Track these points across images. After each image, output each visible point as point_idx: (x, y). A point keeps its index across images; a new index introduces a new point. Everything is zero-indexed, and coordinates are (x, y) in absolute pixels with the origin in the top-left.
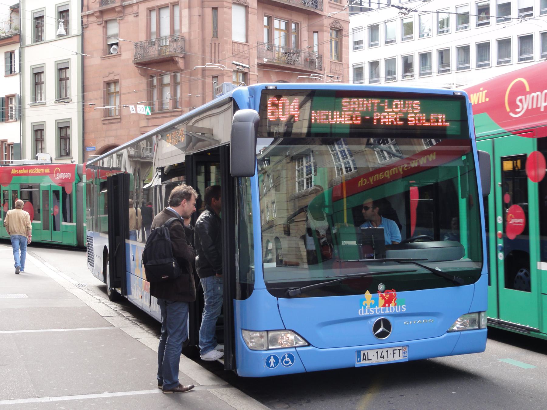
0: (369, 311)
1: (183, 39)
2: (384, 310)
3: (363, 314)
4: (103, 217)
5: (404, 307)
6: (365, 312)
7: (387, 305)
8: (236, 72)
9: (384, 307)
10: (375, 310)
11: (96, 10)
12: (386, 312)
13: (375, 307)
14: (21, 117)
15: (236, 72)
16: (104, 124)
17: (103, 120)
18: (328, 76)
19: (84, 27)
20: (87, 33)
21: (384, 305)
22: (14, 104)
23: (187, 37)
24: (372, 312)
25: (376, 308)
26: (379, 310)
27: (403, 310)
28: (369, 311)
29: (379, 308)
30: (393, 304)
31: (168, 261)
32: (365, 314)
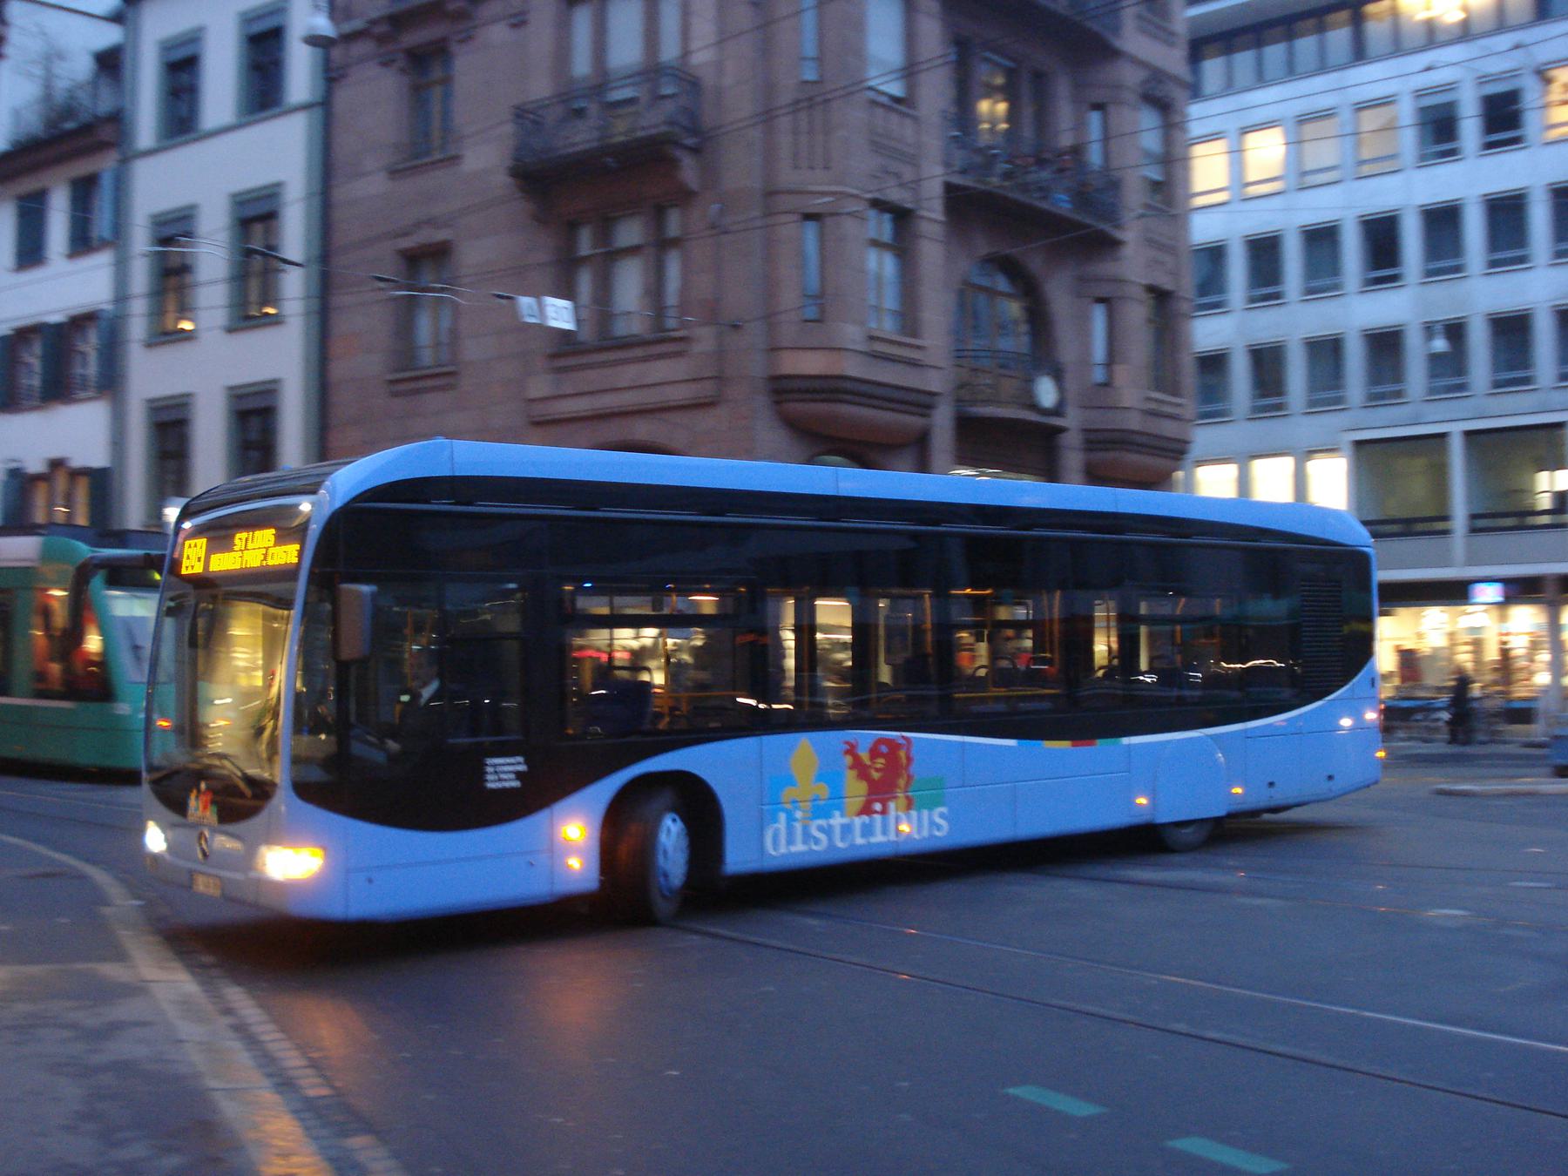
0: (807, 836)
1: (692, 84)
2: (867, 831)
3: (783, 850)
4: (833, 713)
5: (942, 816)
6: (790, 842)
7: (878, 807)
8: (879, 205)
9: (865, 818)
10: (828, 831)
11: (374, 14)
12: (873, 840)
13: (828, 816)
14: (111, 383)
15: (879, 205)
16: (396, 395)
17: (392, 382)
18: (1376, 782)
19: (331, 76)
20: (345, 96)
21: (866, 810)
22: (90, 345)
23: (708, 78)
24: (817, 841)
25: (837, 820)
26: (847, 830)
27: (939, 827)
28: (807, 836)
29: (845, 820)
30: (902, 801)
31: (398, 708)
32: (793, 849)
